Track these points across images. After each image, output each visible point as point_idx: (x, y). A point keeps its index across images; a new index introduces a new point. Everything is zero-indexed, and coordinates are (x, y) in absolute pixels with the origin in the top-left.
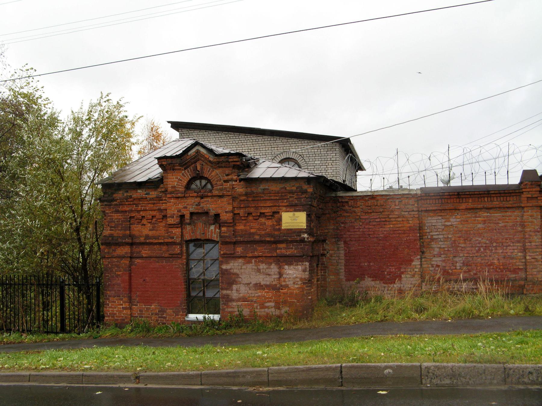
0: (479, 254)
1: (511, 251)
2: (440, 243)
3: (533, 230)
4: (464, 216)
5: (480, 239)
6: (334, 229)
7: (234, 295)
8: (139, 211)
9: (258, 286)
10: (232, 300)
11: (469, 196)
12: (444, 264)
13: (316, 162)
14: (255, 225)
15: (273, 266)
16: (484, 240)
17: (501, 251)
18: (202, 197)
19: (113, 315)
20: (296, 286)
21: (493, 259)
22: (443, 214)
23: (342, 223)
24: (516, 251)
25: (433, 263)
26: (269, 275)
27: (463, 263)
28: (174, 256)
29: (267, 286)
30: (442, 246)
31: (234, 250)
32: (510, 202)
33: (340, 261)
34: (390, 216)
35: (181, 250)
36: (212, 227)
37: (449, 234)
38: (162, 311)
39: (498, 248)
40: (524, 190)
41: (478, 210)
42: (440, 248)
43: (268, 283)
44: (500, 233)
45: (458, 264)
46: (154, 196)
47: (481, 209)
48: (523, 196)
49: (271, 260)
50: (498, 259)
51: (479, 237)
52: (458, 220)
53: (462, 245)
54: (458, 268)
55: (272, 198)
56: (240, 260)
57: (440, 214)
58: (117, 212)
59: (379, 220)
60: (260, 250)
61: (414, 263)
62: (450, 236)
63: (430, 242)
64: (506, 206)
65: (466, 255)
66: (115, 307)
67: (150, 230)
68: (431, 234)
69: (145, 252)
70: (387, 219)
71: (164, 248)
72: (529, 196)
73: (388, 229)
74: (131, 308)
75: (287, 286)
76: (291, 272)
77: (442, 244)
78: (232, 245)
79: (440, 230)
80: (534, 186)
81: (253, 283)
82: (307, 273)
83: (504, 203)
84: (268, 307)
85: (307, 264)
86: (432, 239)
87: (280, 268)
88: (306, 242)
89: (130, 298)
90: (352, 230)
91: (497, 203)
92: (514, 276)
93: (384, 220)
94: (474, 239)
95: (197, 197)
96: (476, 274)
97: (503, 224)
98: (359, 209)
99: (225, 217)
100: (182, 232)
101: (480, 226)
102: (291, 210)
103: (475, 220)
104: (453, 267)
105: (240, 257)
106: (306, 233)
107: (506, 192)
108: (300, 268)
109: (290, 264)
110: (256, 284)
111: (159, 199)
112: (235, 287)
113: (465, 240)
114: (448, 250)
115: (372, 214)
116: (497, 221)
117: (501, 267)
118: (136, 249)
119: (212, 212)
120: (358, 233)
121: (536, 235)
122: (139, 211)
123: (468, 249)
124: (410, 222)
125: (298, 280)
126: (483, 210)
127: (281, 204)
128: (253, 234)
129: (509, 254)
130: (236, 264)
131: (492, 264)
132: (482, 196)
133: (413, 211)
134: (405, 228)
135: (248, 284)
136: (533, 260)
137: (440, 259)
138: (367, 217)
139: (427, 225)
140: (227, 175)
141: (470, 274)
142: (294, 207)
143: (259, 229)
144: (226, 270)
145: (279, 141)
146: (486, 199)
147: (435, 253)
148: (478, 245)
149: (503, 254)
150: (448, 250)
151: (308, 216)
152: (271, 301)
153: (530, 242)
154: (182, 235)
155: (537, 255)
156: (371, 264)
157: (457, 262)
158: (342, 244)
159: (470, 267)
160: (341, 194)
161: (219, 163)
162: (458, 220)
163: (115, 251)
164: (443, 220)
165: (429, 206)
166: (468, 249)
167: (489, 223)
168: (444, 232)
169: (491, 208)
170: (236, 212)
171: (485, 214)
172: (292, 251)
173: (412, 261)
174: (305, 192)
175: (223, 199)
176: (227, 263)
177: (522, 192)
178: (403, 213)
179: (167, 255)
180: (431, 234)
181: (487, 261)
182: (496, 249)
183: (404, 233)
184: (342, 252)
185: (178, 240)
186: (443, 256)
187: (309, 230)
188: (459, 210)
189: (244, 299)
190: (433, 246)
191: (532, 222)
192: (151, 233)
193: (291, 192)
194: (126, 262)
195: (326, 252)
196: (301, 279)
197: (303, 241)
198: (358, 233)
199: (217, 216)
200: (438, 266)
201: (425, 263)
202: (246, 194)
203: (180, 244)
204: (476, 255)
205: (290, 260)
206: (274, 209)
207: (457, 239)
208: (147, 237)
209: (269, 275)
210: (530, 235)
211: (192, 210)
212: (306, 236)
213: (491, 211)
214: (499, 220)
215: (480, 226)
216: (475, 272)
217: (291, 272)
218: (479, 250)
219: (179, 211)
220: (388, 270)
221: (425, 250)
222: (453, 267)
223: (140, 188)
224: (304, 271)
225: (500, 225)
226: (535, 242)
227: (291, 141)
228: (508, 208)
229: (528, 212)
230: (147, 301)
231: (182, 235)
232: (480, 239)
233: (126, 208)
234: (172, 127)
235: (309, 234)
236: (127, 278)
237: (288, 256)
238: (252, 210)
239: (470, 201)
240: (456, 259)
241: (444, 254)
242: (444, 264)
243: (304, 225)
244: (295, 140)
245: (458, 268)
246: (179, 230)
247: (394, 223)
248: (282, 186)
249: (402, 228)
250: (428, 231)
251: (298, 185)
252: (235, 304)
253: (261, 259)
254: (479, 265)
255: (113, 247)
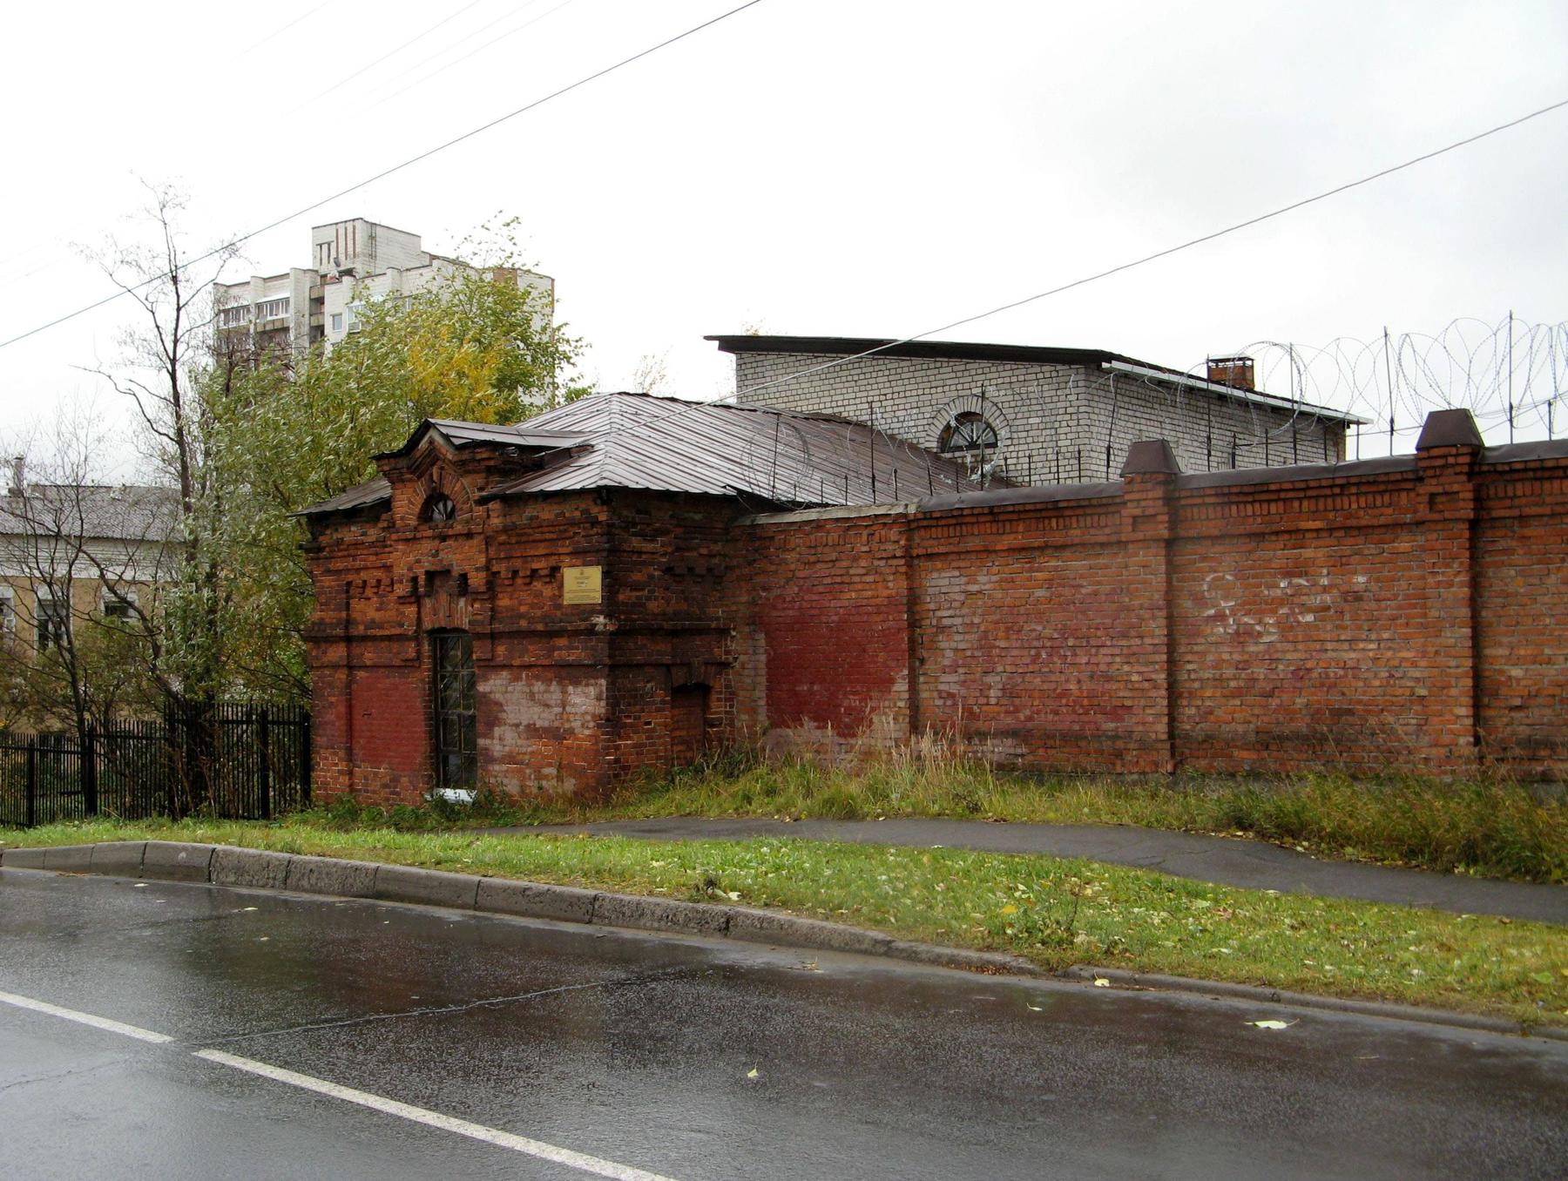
0: (1037, 667)
1: (1109, 659)
2: (958, 637)
3: (1147, 604)
4: (1006, 569)
5: (1039, 628)
6: (748, 602)
7: (497, 749)
8: (358, 570)
9: (533, 731)
10: (493, 760)
11: (1015, 517)
12: (963, 692)
13: (1031, 421)
14: (525, 596)
15: (554, 687)
16: (1047, 632)
17: (1084, 660)
18: (444, 538)
19: (325, 785)
20: (587, 732)
21: (1067, 681)
22: (962, 564)
23: (764, 589)
24: (1118, 659)
25: (942, 687)
26: (548, 706)
27: (1003, 689)
28: (412, 664)
29: (546, 730)
30: (961, 646)
31: (493, 651)
32: (1107, 531)
33: (758, 679)
34: (852, 572)
35: (418, 652)
36: (462, 602)
37: (974, 614)
38: (395, 780)
39: (1078, 651)
40: (1127, 497)
41: (1036, 553)
42: (956, 650)
43: (546, 724)
44: (1084, 613)
45: (992, 693)
46: (373, 539)
47: (1042, 548)
48: (1124, 512)
49: (550, 675)
50: (1079, 682)
51: (1039, 623)
52: (994, 578)
53: (1003, 644)
54: (993, 701)
55: (548, 536)
56: (505, 674)
57: (955, 564)
58: (328, 572)
59: (828, 580)
60: (533, 652)
61: (896, 688)
62: (976, 621)
63: (936, 634)
64: (1094, 540)
65: (1009, 669)
66: (329, 769)
67: (378, 610)
68: (939, 614)
69: (369, 655)
70: (846, 579)
71: (395, 646)
72: (1138, 512)
73: (846, 603)
74: (351, 773)
75: (571, 731)
76: (578, 700)
77: (960, 641)
78: (488, 642)
79: (955, 604)
80: (1149, 486)
81: (525, 723)
82: (603, 703)
83: (1093, 531)
84: (546, 777)
85: (603, 682)
86: (942, 629)
87: (564, 692)
88: (597, 634)
89: (350, 752)
90: (780, 606)
91: (1078, 532)
92: (1112, 725)
93: (838, 580)
94: (1026, 628)
95: (434, 538)
96: (1030, 719)
97: (1089, 589)
98: (793, 554)
99: (477, 580)
100: (419, 613)
101: (1040, 593)
102: (579, 562)
103: (1030, 579)
104: (982, 701)
105: (504, 667)
106: (601, 613)
107: (1028, 507)
108: (592, 691)
109: (576, 683)
110: (528, 726)
111: (381, 544)
112: (497, 731)
113: (1008, 629)
114: (973, 657)
115: (819, 566)
116: (1078, 581)
117: (1086, 702)
118: (357, 650)
119: (456, 571)
120: (791, 613)
121: (1154, 618)
122: (358, 570)
123: (1015, 652)
124: (891, 585)
125: (589, 718)
126: (1049, 552)
127: (561, 550)
128: (521, 616)
129: (1103, 667)
130: (499, 682)
131: (1065, 693)
132: (1044, 514)
133: (894, 557)
134: (878, 601)
135: (517, 725)
136: (1146, 685)
137: (953, 678)
138: (806, 573)
139: (930, 591)
140: (481, 489)
141: (1018, 719)
142: (582, 556)
143: (532, 606)
144: (484, 695)
145: (948, 370)
146: (1054, 522)
147: (947, 662)
148: (1036, 643)
149: (1089, 668)
150: (973, 657)
151: (605, 574)
152: (550, 765)
153: (1142, 637)
154: (419, 620)
155: (1155, 671)
156: (815, 688)
157: (990, 687)
158: (761, 637)
159: (1017, 701)
160: (763, 519)
161: (463, 463)
162: (994, 578)
163: (325, 653)
164: (964, 580)
165: (935, 542)
166: (1015, 652)
167: (1060, 585)
168: (965, 611)
169: (1063, 547)
170: (495, 569)
171: (1053, 563)
172: (573, 652)
173: (892, 681)
174: (595, 523)
175: (470, 542)
176: (487, 680)
177: (1125, 503)
178: (876, 563)
179: (397, 662)
180: (939, 614)
181: (1053, 686)
182: (1075, 655)
183: (878, 613)
184: (763, 658)
185: (410, 629)
186: (961, 670)
187: (610, 605)
188: (995, 552)
189: (510, 758)
190: (943, 645)
191: (1145, 582)
192: (377, 616)
193: (573, 523)
194: (342, 675)
195: (731, 659)
196: (594, 716)
197: (591, 631)
198: (791, 613)
199: (464, 577)
200: (951, 696)
201: (925, 687)
202: (505, 530)
203: (416, 638)
204: (1031, 668)
205: (570, 673)
206: (553, 561)
207: (991, 627)
208: (372, 624)
209: (548, 706)
210: (1141, 619)
211: (427, 566)
212: (601, 619)
213: (1067, 554)
214: (1082, 577)
215: (1040, 593)
216: (1028, 712)
217: (578, 700)
218: (1038, 655)
219: (410, 569)
220: (846, 703)
221: (925, 654)
222: (982, 701)
223: (354, 523)
224: (599, 699)
225: (1084, 591)
226: (1153, 637)
227: (974, 366)
228: (1102, 545)
229: (1136, 555)
230: (376, 763)
231: (419, 620)
232: (1039, 628)
233: (340, 565)
234: (721, 348)
235: (608, 616)
236: (342, 709)
237: (570, 666)
238: (518, 564)
239: (1021, 528)
240: (990, 679)
241: (964, 666)
242: (963, 692)
243: (596, 596)
244: (985, 364)
245: (993, 701)
246: (414, 609)
247: (860, 587)
248: (557, 509)
249: (873, 601)
250: (932, 606)
251: (583, 506)
252: (497, 768)
253: (535, 671)
254: (1036, 694)
255: (323, 646)
